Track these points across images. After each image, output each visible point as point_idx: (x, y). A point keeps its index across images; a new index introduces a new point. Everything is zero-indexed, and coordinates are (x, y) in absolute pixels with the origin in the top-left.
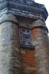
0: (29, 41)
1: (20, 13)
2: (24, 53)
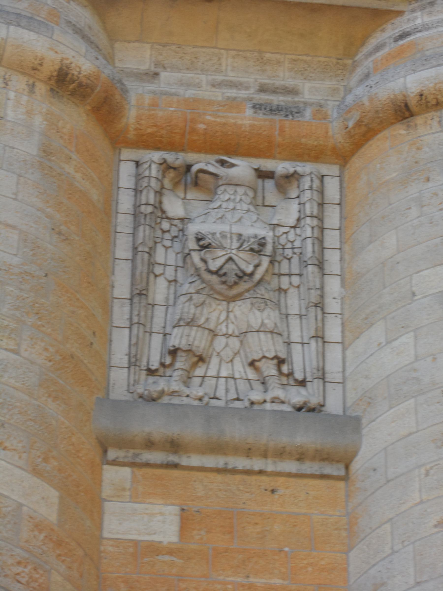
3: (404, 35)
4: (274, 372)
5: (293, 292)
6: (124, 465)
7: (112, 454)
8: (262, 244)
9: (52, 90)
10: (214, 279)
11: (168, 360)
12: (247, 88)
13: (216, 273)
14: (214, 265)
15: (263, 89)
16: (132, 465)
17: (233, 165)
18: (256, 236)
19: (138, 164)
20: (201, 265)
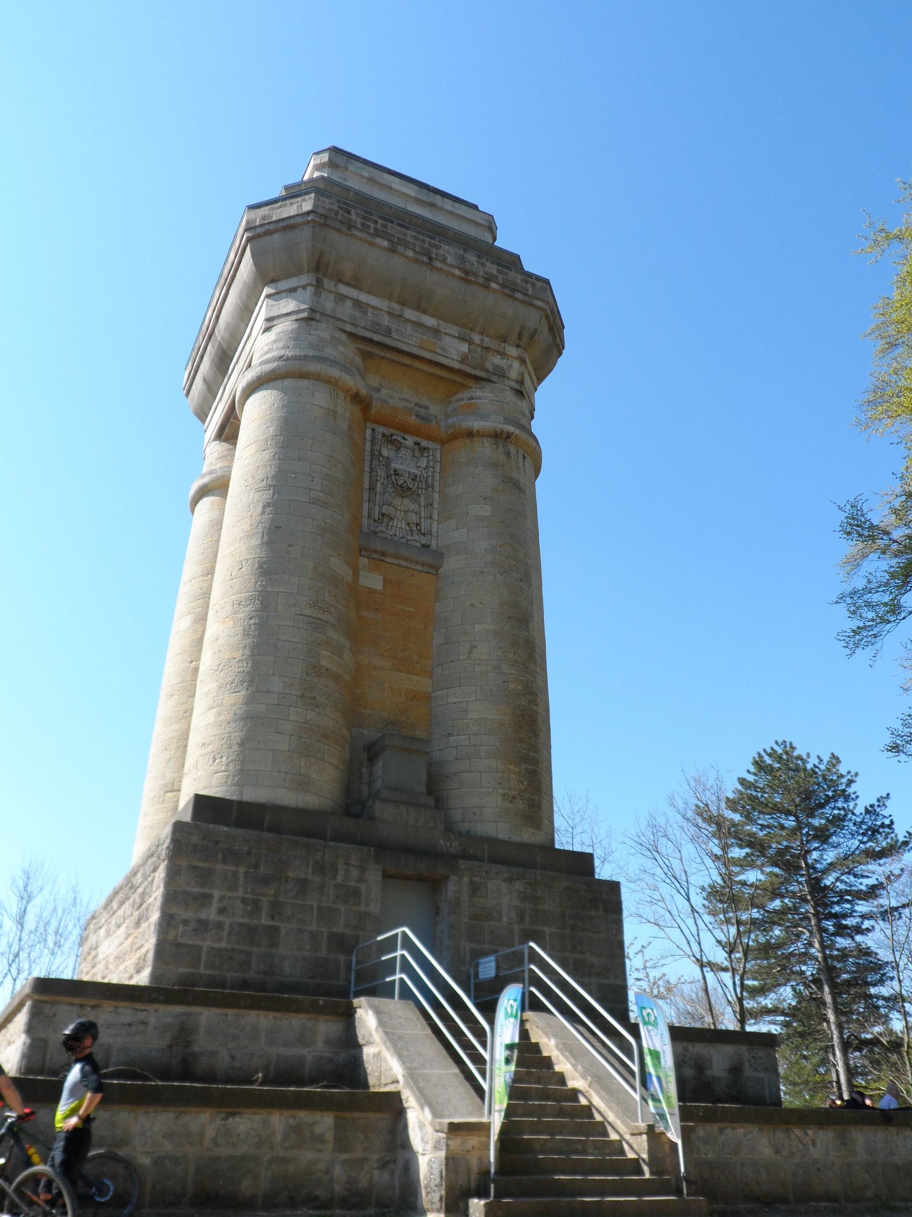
0: (414, 518)
1: (386, 320)
2: (378, 584)
3: (471, 398)
4: (415, 529)
5: (422, 496)
6: (366, 557)
7: (363, 553)
8: (416, 477)
9: (351, 400)
10: (399, 488)
11: (381, 517)
12: (411, 403)
13: (400, 486)
14: (400, 483)
15: (417, 405)
16: (369, 558)
17: (407, 440)
18: (414, 473)
19: (373, 430)
20: (395, 481)
